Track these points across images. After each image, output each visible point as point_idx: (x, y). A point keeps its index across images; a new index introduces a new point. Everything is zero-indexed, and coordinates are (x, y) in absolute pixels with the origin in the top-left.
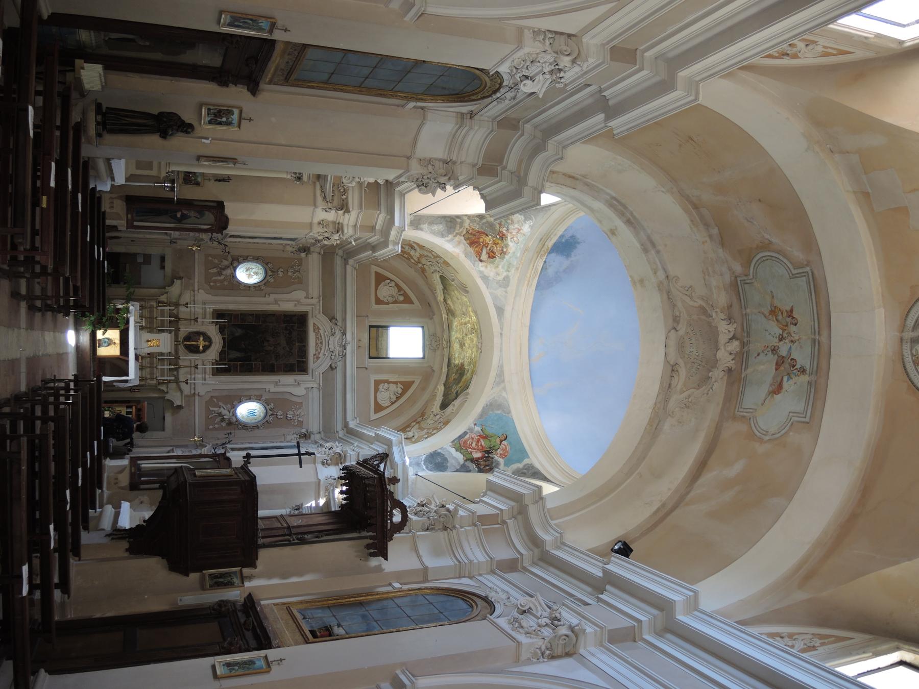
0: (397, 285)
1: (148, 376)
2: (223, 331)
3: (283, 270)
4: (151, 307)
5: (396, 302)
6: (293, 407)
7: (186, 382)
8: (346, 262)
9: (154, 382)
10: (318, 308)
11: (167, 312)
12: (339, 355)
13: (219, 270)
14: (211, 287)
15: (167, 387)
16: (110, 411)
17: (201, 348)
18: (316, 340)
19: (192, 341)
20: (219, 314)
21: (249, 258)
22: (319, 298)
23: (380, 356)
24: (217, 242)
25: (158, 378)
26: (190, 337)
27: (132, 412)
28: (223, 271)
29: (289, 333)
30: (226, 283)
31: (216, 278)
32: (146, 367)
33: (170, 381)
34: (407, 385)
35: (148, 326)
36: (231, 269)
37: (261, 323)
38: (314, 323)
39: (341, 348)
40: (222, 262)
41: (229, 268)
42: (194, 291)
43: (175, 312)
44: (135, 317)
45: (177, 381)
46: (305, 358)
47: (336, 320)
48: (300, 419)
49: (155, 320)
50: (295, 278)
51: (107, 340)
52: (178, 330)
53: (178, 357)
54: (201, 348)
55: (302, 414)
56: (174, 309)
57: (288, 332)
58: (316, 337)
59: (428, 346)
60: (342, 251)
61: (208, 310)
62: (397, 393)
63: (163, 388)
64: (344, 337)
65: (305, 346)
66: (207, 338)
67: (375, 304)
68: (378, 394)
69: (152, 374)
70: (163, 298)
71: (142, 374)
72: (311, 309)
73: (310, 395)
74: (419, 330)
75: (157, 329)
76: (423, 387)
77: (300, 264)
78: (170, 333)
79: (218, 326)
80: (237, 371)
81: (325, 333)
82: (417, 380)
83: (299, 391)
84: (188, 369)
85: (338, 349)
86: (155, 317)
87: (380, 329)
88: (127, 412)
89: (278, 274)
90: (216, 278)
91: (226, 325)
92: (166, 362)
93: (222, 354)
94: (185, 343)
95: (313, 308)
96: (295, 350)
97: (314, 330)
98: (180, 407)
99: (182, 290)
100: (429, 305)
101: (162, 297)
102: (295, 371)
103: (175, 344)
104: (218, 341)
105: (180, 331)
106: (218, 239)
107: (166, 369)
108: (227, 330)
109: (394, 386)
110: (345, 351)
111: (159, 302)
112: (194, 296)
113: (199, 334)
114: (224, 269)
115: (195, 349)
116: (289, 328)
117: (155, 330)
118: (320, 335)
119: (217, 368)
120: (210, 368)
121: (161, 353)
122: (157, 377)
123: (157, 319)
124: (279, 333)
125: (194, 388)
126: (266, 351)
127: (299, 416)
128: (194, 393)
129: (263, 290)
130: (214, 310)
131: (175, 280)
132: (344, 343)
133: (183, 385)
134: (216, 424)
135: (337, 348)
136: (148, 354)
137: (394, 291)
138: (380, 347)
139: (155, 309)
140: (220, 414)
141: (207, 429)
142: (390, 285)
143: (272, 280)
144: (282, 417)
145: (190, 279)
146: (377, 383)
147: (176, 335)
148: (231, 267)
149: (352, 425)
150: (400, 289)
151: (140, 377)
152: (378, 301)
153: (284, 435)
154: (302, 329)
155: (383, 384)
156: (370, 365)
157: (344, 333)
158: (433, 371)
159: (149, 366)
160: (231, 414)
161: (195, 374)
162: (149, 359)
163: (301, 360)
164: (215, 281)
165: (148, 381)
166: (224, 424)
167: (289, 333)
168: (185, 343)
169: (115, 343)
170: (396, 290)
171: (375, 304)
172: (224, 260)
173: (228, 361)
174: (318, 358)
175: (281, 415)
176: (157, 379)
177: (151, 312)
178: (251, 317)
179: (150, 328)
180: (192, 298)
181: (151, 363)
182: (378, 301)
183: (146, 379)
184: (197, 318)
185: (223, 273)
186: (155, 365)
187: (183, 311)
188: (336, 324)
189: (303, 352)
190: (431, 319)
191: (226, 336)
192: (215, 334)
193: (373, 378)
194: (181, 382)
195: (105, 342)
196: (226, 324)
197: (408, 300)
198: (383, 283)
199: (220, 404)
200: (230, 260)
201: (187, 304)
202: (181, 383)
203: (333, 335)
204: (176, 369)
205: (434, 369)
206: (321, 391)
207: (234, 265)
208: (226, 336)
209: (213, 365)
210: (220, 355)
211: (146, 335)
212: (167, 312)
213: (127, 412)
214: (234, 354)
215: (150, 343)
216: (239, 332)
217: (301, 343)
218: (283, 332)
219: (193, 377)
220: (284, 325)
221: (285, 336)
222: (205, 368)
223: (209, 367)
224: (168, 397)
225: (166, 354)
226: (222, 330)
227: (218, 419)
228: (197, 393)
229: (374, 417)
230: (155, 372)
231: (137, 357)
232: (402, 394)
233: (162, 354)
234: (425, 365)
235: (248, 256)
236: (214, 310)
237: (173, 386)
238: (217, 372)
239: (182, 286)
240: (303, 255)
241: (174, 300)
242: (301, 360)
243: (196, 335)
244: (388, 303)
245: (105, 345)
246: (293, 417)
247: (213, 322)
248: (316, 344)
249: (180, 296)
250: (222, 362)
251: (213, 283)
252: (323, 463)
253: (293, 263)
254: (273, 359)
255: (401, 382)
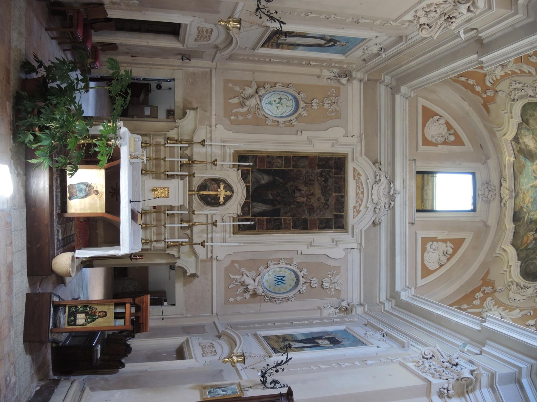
0: (447, 123)
1: (154, 238)
2: (246, 177)
3: (317, 101)
4: (158, 145)
5: (445, 143)
6: (329, 273)
7: (203, 244)
8: (394, 91)
9: (162, 245)
10: (359, 148)
11: (178, 153)
12: (385, 208)
13: (241, 99)
14: (232, 122)
15: (179, 251)
16: (87, 314)
17: (222, 200)
18: (356, 190)
19: (209, 191)
20: (242, 157)
21: (277, 85)
22: (360, 136)
23: (425, 209)
24: (267, 15)
25: (167, 240)
26: (207, 185)
27: (124, 313)
28: (246, 100)
29: (324, 181)
30: (250, 117)
31: (237, 110)
32: (151, 226)
33: (181, 244)
34: (457, 244)
35: (154, 170)
36: (256, 98)
37: (291, 168)
38: (354, 169)
39: (387, 200)
40: (244, 89)
41: (254, 97)
42: (211, 127)
43: (188, 152)
44: (130, 147)
45: (191, 243)
46: (344, 211)
47: (380, 164)
48: (337, 288)
49: (162, 161)
50: (332, 112)
51: (84, 187)
52: (192, 175)
53: (192, 212)
54: (222, 200)
55: (340, 281)
56: (187, 148)
57: (323, 179)
58: (357, 186)
59: (481, 197)
60: (390, 78)
61: (228, 151)
62: (446, 253)
63: (173, 251)
64: (392, 185)
65: (343, 197)
66: (229, 187)
67: (422, 145)
68: (426, 254)
69: (158, 234)
70: (173, 134)
71: (146, 236)
72: (350, 150)
73: (350, 258)
74: (469, 178)
75: (165, 175)
76: (476, 247)
77: (338, 95)
78: (182, 179)
79: (240, 172)
80: (263, 229)
81: (368, 180)
82: (469, 237)
83: (337, 253)
84: (204, 227)
85: (384, 201)
86: (162, 157)
87: (426, 176)
88: (115, 313)
89: (312, 106)
90: (237, 110)
91: (250, 170)
92: (176, 218)
93: (245, 206)
94: (202, 193)
95: (353, 148)
96: (332, 202)
97: (354, 176)
98: (194, 276)
99: (196, 124)
100: (481, 147)
101: (171, 132)
102: (332, 228)
103: (189, 195)
104: (240, 191)
105: (194, 177)
106: (268, 12)
107: (177, 236)
108: (250, 177)
109: (444, 244)
110: (392, 203)
111: (168, 139)
112: (211, 134)
113: (217, 181)
114: (247, 99)
115: (213, 201)
116: (324, 174)
117: (162, 175)
118: (361, 183)
119: (239, 225)
120: (230, 225)
121: (171, 206)
122: (165, 239)
123: (165, 161)
124: (313, 180)
125: (212, 251)
126: (298, 203)
127: (336, 284)
128: (212, 257)
129: (293, 126)
130: (235, 151)
131: (188, 111)
132: (392, 193)
133: (199, 249)
134: (237, 295)
135: (383, 199)
136: (154, 207)
137: (444, 130)
138: (425, 197)
139: (162, 148)
140: (243, 284)
141: (227, 302)
142: (440, 122)
143: (305, 114)
144: (316, 285)
145: (206, 111)
146: (425, 241)
147: (190, 183)
148: (257, 95)
149: (404, 296)
150: (449, 127)
151: (143, 239)
152: (426, 142)
153: (320, 308)
154: (339, 176)
155: (430, 243)
156: (416, 219)
157: (392, 181)
158: (487, 226)
159: (155, 223)
160: (256, 284)
161: (212, 232)
162: (155, 214)
163: (339, 213)
164: (236, 115)
165: (155, 244)
166: (247, 296)
167: (324, 181)
168: (202, 193)
169: (97, 192)
170: (446, 129)
171: (422, 145)
172: (246, 88)
173: (252, 217)
174: (359, 212)
175: (316, 283)
176: (165, 242)
177: (158, 151)
178: (279, 160)
179: (156, 173)
180: (209, 136)
181: (158, 220)
182: (426, 142)
183: (152, 242)
184: (216, 160)
185: (246, 104)
186: (163, 223)
187: (198, 152)
188: (380, 169)
189: (341, 204)
190: (484, 163)
191: (250, 185)
192: (236, 181)
193: (421, 235)
194: (196, 244)
195: (81, 191)
196: (250, 169)
197: (458, 142)
198: (431, 120)
199: (243, 270)
200: (255, 87)
201: (204, 141)
202: (195, 246)
203: (376, 182)
204: (190, 227)
205: (489, 223)
206: (363, 253)
207: (260, 94)
208: (250, 185)
209: (234, 222)
210: (243, 208)
211: (151, 182)
212: (178, 153)
213: (115, 313)
214: (260, 207)
215: (156, 193)
216: (265, 179)
217: (339, 192)
218: (318, 179)
219: (210, 236)
220: (318, 171)
221: (320, 184)
222: (225, 226)
223: (230, 224)
224: (179, 263)
225: (176, 208)
226: (245, 176)
227: (242, 289)
228: (214, 256)
229: (421, 282)
230: (163, 231)
231: (134, 216)
232: (452, 255)
233: (171, 208)
234: (477, 219)
235: (276, 83)
236: (235, 151)
237: (185, 249)
238: (240, 230)
239: (196, 120)
240: (344, 80)
241: (186, 138)
242: (339, 213)
243: (213, 182)
244: (436, 145)
245: (82, 195)
246: (330, 285)
247: (234, 166)
248: (357, 194)
249: (194, 132)
250: (244, 217)
251: (234, 116)
252: (441, 395)
253: (329, 93)
254: (306, 212)
255: (452, 241)
